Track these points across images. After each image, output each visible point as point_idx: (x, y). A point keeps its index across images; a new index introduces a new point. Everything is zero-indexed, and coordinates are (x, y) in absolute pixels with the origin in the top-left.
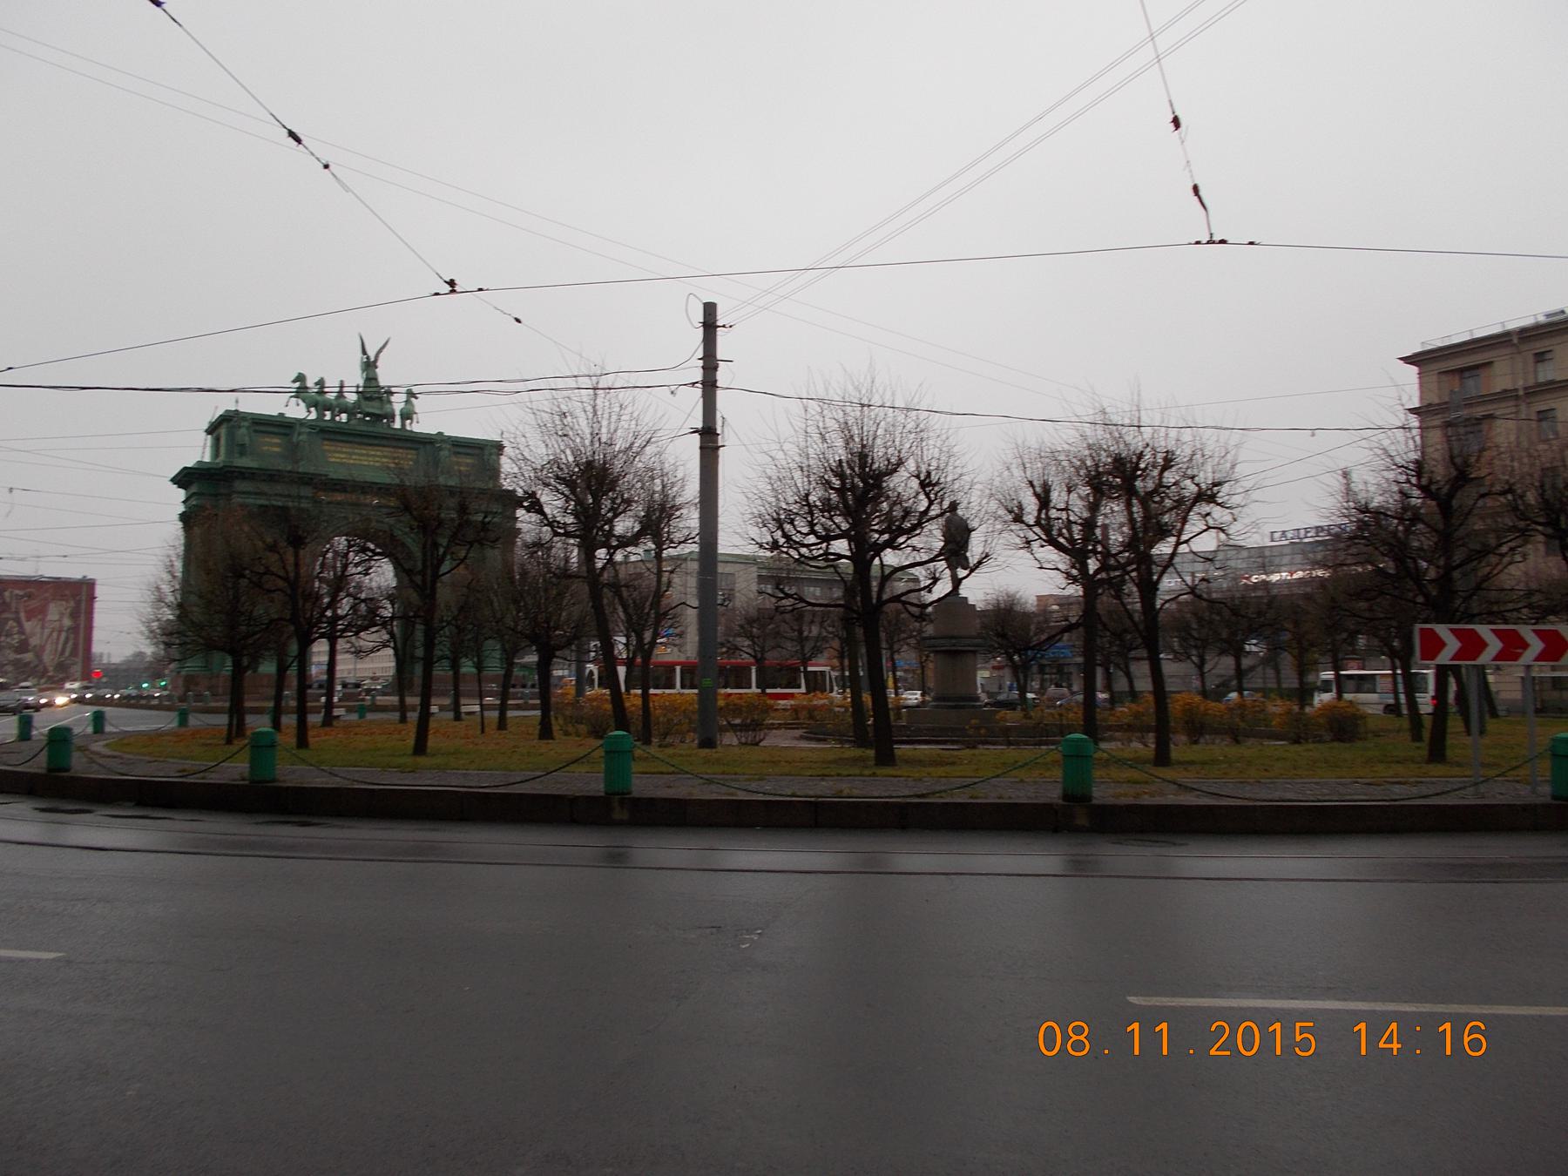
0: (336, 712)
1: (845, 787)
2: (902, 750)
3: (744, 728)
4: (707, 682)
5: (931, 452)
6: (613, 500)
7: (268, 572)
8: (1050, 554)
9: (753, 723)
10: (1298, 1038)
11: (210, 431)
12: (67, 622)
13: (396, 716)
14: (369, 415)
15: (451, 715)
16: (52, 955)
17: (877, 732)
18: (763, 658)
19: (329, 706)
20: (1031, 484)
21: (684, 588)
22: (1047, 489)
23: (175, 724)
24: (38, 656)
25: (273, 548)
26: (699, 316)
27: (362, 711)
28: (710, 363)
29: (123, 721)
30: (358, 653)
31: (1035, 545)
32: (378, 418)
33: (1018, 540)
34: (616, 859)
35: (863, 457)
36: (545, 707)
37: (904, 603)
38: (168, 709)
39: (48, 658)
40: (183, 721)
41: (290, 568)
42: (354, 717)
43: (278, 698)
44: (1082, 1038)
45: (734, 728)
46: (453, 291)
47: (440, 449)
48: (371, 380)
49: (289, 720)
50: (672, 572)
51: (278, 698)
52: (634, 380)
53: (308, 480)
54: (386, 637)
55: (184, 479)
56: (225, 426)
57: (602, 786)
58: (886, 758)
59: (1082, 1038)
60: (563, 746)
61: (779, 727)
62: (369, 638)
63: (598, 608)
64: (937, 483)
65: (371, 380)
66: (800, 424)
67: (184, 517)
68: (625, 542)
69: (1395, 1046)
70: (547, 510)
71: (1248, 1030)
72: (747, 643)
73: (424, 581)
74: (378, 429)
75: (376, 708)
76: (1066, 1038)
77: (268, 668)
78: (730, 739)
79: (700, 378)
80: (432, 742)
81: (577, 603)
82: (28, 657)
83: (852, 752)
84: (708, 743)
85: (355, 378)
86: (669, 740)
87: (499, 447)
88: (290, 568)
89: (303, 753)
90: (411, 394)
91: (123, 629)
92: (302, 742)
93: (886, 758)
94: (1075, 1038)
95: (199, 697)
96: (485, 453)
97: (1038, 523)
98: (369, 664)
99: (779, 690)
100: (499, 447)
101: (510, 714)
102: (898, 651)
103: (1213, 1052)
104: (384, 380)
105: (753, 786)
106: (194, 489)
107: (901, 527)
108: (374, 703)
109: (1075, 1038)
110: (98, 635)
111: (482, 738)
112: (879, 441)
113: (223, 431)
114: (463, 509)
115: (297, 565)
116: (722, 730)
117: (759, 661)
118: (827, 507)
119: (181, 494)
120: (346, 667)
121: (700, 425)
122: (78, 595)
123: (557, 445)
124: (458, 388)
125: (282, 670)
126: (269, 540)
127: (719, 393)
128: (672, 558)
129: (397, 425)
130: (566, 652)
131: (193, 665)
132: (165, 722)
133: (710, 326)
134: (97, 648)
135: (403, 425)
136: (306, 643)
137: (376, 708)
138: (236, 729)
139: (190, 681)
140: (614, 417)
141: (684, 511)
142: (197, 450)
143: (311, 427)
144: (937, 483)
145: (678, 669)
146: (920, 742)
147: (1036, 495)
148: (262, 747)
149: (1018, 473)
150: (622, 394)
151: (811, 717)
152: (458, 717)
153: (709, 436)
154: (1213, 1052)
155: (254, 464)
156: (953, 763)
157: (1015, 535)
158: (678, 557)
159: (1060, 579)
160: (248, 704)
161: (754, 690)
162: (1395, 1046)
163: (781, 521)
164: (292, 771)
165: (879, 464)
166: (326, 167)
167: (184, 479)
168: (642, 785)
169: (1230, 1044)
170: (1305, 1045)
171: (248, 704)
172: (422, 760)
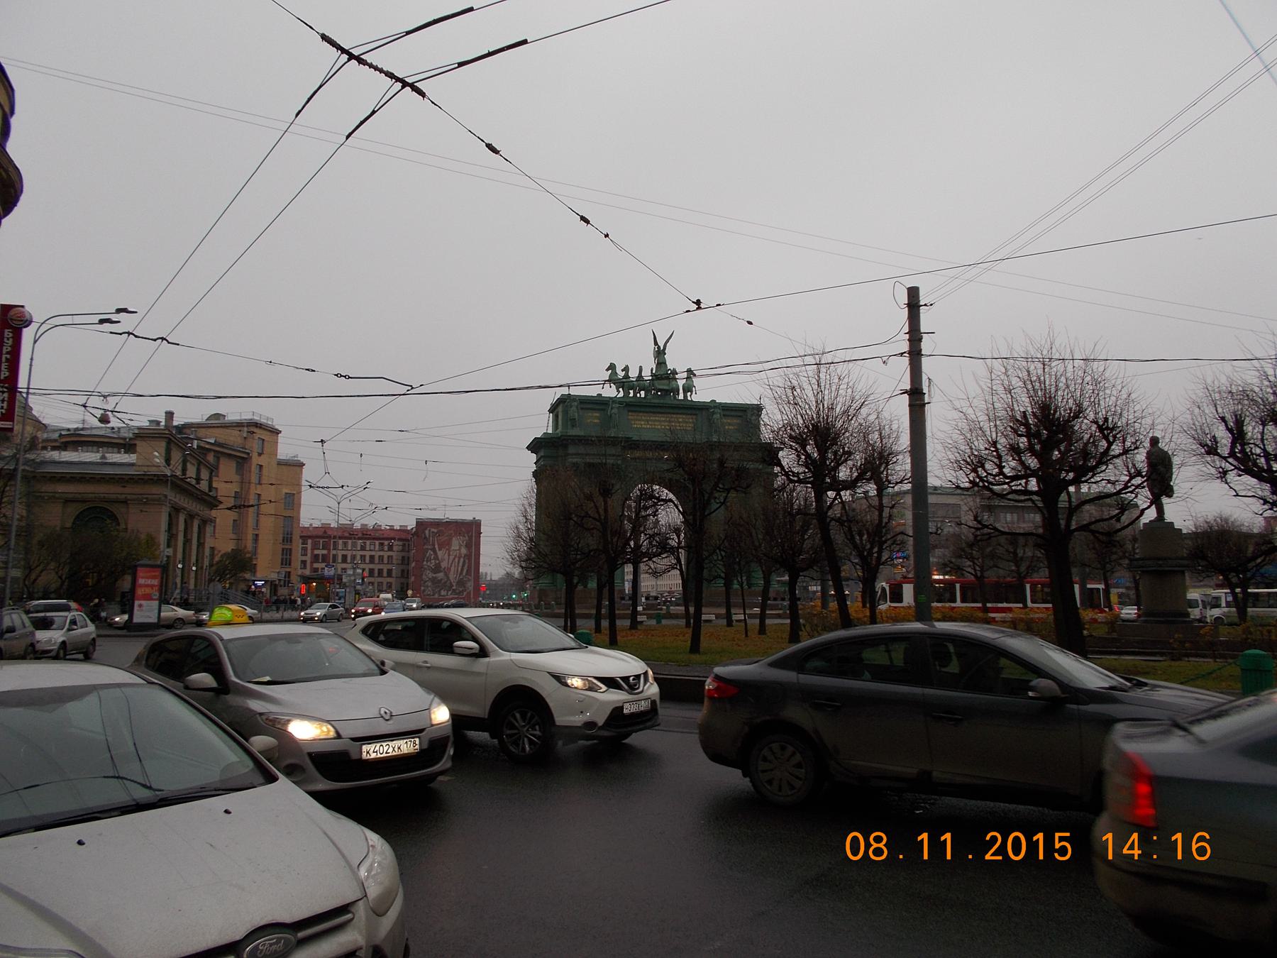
0: (640, 618)
6: (835, 453)
7: (587, 515)
8: (1248, 482)
10: (1057, 846)
11: (550, 411)
12: (464, 551)
14: (659, 391)
15: (724, 622)
19: (635, 613)
20: (1223, 419)
22: (1239, 423)
24: (447, 575)
26: (904, 299)
27: (659, 618)
28: (915, 335)
30: (656, 574)
31: (1231, 476)
32: (666, 392)
33: (1213, 471)
35: (1045, 410)
37: (1093, 532)
39: (452, 576)
42: (653, 622)
43: (599, 607)
47: (713, 413)
48: (661, 363)
50: (893, 507)
51: (599, 607)
52: (849, 355)
53: (614, 442)
55: (535, 446)
56: (563, 407)
62: (664, 561)
65: (661, 363)
66: (985, 383)
67: (535, 474)
68: (851, 485)
69: (1137, 852)
70: (784, 463)
72: (969, 563)
73: (695, 520)
74: (668, 401)
76: (868, 845)
79: (906, 348)
80: (704, 643)
82: (440, 575)
87: (758, 409)
96: (748, 414)
97: (1232, 454)
99: (1005, 605)
103: (988, 857)
113: (560, 409)
115: (606, 510)
118: (1015, 450)
119: (534, 457)
120: (648, 584)
121: (908, 387)
124: (715, 372)
125: (600, 587)
126: (587, 491)
129: (681, 397)
131: (545, 581)
133: (914, 305)
135: (685, 396)
141: (900, 457)
142: (543, 425)
143: (620, 403)
145: (958, 586)
147: (1229, 430)
149: (1209, 410)
150: (840, 367)
152: (730, 624)
153: (916, 396)
155: (582, 433)
157: (1209, 466)
159: (1257, 506)
160: (577, 611)
165: (1062, 413)
166: (607, 236)
167: (535, 446)
169: (1002, 850)
170: (1063, 851)
171: (577, 611)
172: (695, 657)
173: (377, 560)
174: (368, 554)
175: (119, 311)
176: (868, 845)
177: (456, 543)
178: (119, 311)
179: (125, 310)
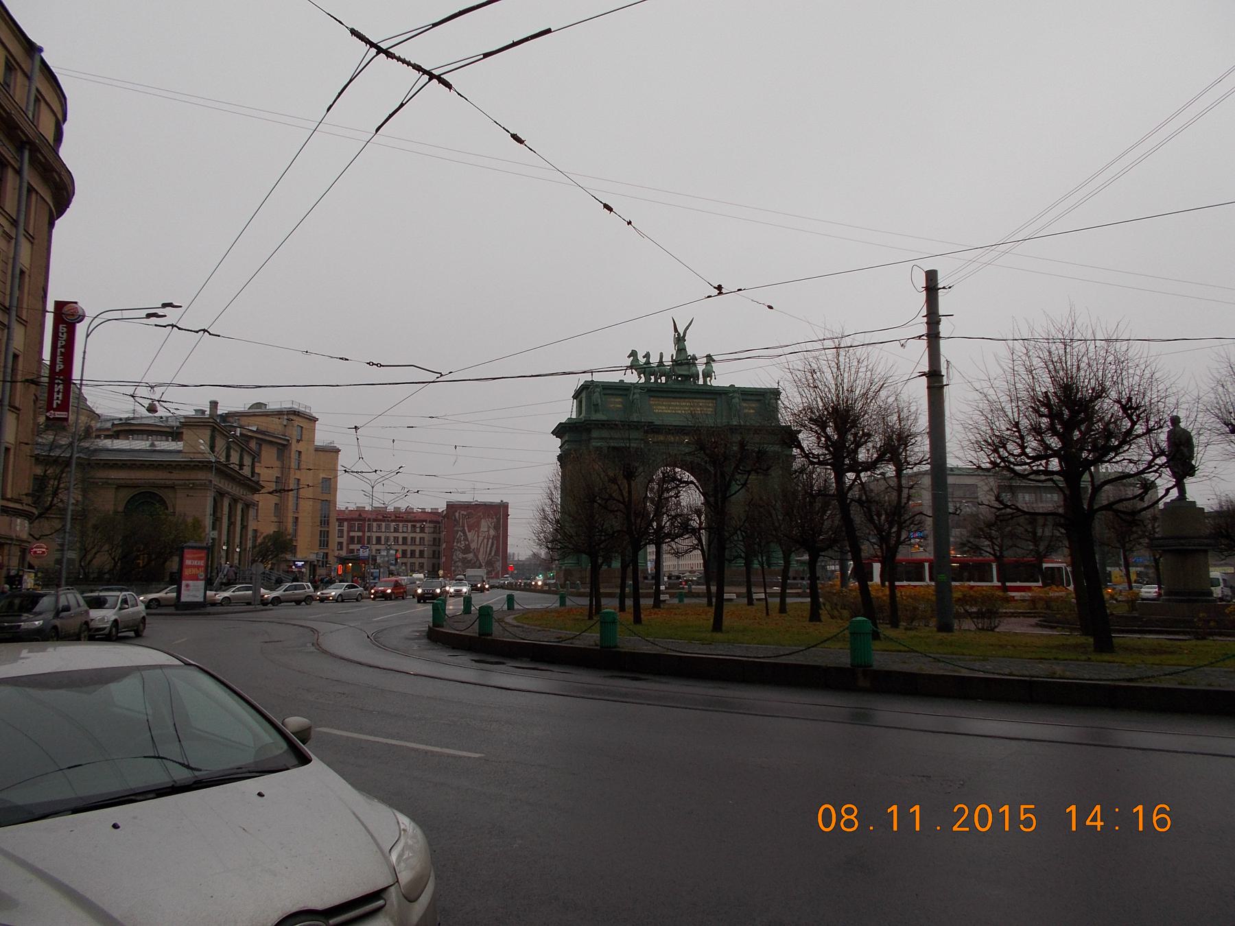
0: (662, 597)
1: (1058, 669)
2: (1119, 638)
3: (980, 615)
4: (942, 577)
5: (1131, 381)
6: (855, 435)
9: (989, 611)
10: (1023, 818)
12: (492, 532)
13: (705, 601)
14: (680, 376)
16: (477, 755)
17: (1095, 620)
18: (1002, 556)
19: (658, 592)
21: (924, 499)
23: (557, 605)
24: (476, 556)
25: (613, 480)
26: (922, 282)
27: (681, 597)
28: (933, 319)
29: (525, 601)
30: (677, 554)
32: (686, 378)
34: (861, 718)
35: (1067, 390)
36: (814, 595)
38: (555, 593)
39: (481, 557)
40: (563, 603)
41: (626, 494)
42: (676, 601)
43: (623, 586)
44: (852, 817)
45: (969, 615)
46: (720, 293)
47: (733, 398)
48: (681, 350)
49: (629, 602)
51: (623, 586)
52: (868, 339)
53: (635, 426)
54: (696, 542)
55: (560, 431)
56: (586, 393)
57: (849, 661)
58: (1104, 645)
59: (852, 817)
60: (829, 627)
61: (1013, 615)
62: (686, 542)
63: (847, 519)
64: (1138, 408)
65: (681, 350)
66: (1007, 364)
67: (560, 458)
68: (870, 466)
69: (1099, 824)
70: (804, 445)
71: (983, 811)
72: (987, 543)
74: (688, 386)
75: (691, 594)
76: (839, 817)
77: (616, 564)
78: (968, 624)
79: (924, 331)
80: (727, 621)
81: (831, 519)
82: (470, 556)
83: (1077, 638)
84: (945, 627)
85: (669, 352)
86: (915, 623)
87: (776, 393)
88: (626, 494)
89: (639, 627)
90: (710, 359)
91: (524, 540)
92: (637, 620)
93: (1104, 645)
94: (846, 817)
95: (573, 585)
96: (767, 398)
98: (684, 561)
100: (776, 393)
101: (788, 600)
102: (1131, 550)
103: (955, 828)
104: (690, 352)
105: (977, 665)
106: (566, 438)
107: (1110, 441)
108: (690, 592)
109: (846, 817)
110: (510, 541)
111: (765, 619)
112: (1082, 373)
113: (584, 395)
114: (742, 445)
115: (630, 492)
116: (959, 616)
117: (998, 559)
118: (1036, 430)
119: (558, 442)
120: (670, 564)
121: (926, 369)
122: (498, 513)
123: (810, 395)
125: (624, 567)
126: (611, 474)
127: (942, 342)
128: (910, 476)
129: (701, 382)
130: (830, 553)
131: (570, 562)
132: (551, 602)
134: (510, 550)
136: (638, 547)
137: (691, 594)
138: (595, 609)
139: (568, 574)
140: (853, 370)
141: (919, 438)
142: (567, 410)
144: (1138, 408)
145: (927, 564)
146: (1150, 632)
148: (608, 623)
151: (1048, 607)
153: (934, 378)
154: (955, 828)
156: (1172, 653)
158: (916, 474)
161: (996, 583)
162: (1099, 824)
163: (998, 444)
164: (629, 641)
166: (629, 223)
167: (560, 431)
168: (882, 658)
169: (969, 822)
170: (1028, 823)
172: (718, 636)
173: (409, 541)
174: (400, 536)
175: (165, 305)
176: (839, 817)
177: (485, 525)
178: (165, 305)
179: (170, 305)
